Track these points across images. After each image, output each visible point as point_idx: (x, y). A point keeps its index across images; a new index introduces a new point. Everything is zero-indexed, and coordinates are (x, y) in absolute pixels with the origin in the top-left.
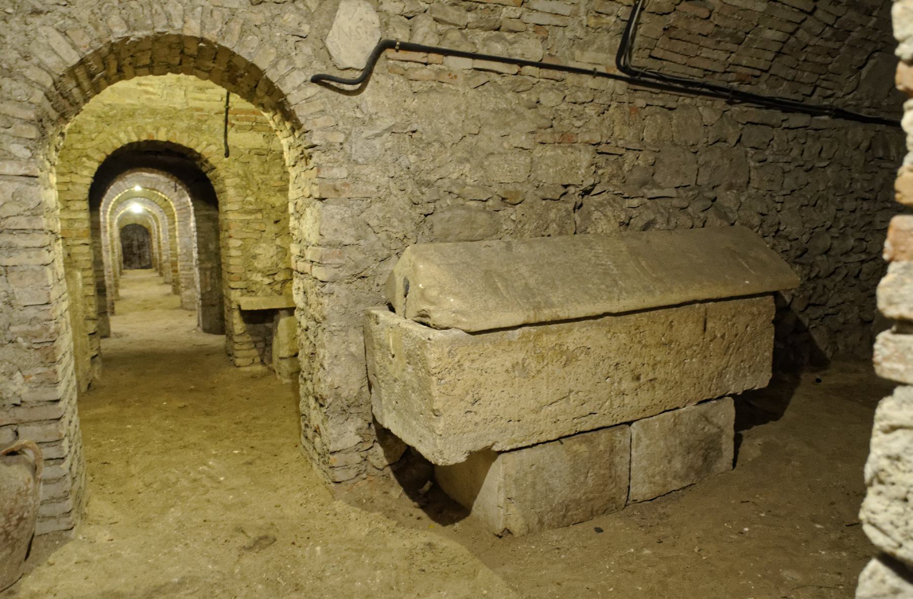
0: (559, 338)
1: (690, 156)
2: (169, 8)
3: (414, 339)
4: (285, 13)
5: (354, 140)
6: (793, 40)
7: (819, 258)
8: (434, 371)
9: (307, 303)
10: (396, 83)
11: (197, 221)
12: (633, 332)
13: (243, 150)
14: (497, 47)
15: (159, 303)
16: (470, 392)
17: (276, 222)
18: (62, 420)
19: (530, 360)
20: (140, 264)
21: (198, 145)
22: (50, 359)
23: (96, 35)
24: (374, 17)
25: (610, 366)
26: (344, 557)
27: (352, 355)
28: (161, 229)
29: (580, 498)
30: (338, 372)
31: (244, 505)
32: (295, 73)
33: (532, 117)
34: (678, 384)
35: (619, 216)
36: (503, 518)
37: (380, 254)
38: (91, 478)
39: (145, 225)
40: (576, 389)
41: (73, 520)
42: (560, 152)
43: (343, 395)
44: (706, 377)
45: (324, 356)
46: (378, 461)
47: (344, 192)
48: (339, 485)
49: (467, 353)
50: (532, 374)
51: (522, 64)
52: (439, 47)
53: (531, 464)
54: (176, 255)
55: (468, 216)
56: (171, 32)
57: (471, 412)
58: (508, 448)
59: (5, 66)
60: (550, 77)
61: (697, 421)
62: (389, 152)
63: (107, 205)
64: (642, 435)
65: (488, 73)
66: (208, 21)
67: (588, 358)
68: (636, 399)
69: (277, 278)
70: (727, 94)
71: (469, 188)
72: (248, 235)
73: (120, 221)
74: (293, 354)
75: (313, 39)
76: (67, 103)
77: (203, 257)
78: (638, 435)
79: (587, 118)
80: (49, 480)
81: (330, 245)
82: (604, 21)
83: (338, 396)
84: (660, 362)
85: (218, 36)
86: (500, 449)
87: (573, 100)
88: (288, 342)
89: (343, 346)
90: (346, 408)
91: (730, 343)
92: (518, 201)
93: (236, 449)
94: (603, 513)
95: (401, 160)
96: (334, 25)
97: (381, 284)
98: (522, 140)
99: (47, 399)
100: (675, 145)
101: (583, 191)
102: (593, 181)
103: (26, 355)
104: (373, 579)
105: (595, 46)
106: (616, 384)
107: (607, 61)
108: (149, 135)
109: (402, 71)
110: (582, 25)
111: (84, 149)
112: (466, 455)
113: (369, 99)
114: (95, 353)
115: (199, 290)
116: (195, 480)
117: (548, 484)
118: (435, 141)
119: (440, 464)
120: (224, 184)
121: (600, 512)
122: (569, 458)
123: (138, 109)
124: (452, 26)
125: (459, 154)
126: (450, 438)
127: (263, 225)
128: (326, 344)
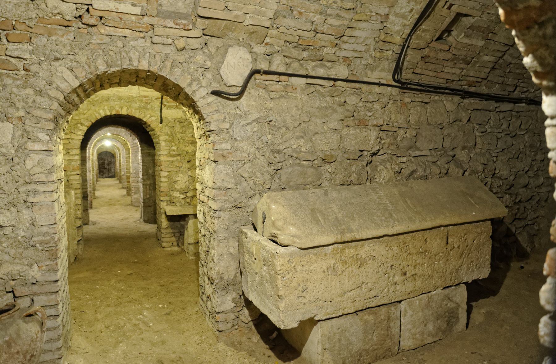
0: (356, 251)
1: (438, 131)
2: (131, 54)
3: (268, 251)
4: (197, 55)
5: (235, 127)
6: (501, 61)
7: (521, 190)
8: (279, 272)
9: (205, 220)
10: (261, 93)
11: (142, 156)
12: (402, 246)
14: (321, 71)
15: (119, 201)
16: (301, 285)
17: (189, 162)
19: (338, 264)
20: (109, 174)
21: (144, 117)
22: (54, 256)
23: (89, 70)
24: (248, 56)
27: (231, 254)
28: (121, 156)
29: (369, 348)
30: (222, 265)
31: (163, 343)
32: (201, 89)
33: (341, 111)
34: (431, 277)
37: (249, 194)
40: (367, 282)
41: (62, 353)
42: (358, 131)
43: (225, 278)
44: (448, 272)
45: (214, 255)
46: (245, 318)
48: (221, 333)
49: (300, 261)
50: (339, 273)
51: (335, 80)
53: (338, 327)
54: (129, 172)
56: (132, 67)
57: (301, 296)
58: (324, 318)
61: (443, 300)
62: (256, 134)
63: (91, 145)
64: (408, 309)
68: (404, 287)
69: (188, 194)
70: (461, 93)
71: (303, 154)
72: (172, 169)
73: (98, 150)
74: (196, 242)
75: (213, 69)
76: (71, 106)
77: (145, 177)
78: (405, 309)
79: (375, 111)
80: (50, 328)
81: (219, 188)
83: (222, 279)
84: (419, 264)
86: (319, 319)
89: (226, 249)
90: (227, 286)
91: (463, 251)
92: (332, 161)
94: (384, 358)
95: (262, 138)
96: (225, 63)
98: (335, 124)
99: (51, 280)
100: (429, 124)
101: (372, 153)
102: (378, 148)
103: (41, 254)
105: (380, 69)
106: (391, 278)
107: (387, 77)
108: (117, 111)
109: (264, 86)
110: (372, 57)
111: (79, 119)
112: (298, 322)
115: (142, 197)
116: (135, 325)
117: (348, 340)
118: (283, 126)
119: (282, 328)
120: (159, 139)
121: (381, 357)
122: (362, 323)
123: (111, 97)
124: (294, 60)
125: (297, 134)
126: (289, 313)
128: (216, 247)
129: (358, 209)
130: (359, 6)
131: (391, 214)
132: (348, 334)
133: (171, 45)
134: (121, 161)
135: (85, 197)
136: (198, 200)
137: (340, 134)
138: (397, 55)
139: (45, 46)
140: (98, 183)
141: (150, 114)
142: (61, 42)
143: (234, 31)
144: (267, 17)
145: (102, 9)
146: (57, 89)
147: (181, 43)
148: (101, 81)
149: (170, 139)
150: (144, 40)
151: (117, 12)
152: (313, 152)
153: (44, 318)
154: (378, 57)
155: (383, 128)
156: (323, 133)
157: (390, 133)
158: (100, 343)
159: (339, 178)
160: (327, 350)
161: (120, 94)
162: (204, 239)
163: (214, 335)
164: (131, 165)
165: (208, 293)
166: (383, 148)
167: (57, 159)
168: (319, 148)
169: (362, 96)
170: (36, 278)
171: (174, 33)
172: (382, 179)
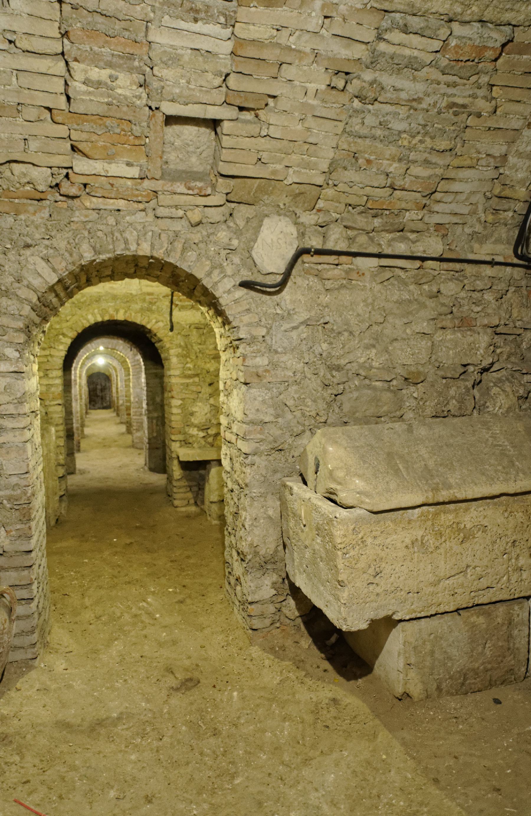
0: (456, 517)
2: (127, 235)
3: (323, 515)
4: (219, 231)
5: (274, 333)
8: (340, 546)
9: (232, 468)
11: (147, 379)
13: (185, 326)
14: (401, 247)
15: (115, 441)
16: (372, 566)
17: (210, 385)
18: (34, 566)
20: (102, 404)
21: (148, 323)
23: (70, 260)
24: (292, 230)
25: (507, 543)
26: (258, 705)
27: (270, 518)
28: (119, 378)
31: (174, 642)
32: (226, 280)
33: (433, 305)
35: (518, 391)
36: (402, 682)
37: (295, 430)
38: (54, 608)
39: (107, 373)
40: (473, 565)
42: (459, 335)
43: (260, 553)
45: (246, 518)
46: (290, 613)
47: (265, 377)
48: (255, 632)
50: (430, 550)
51: (423, 259)
52: (349, 250)
53: (429, 633)
54: (129, 401)
55: (374, 395)
56: (128, 253)
57: (373, 583)
58: (407, 618)
59: (3, 288)
60: (450, 269)
62: (304, 342)
63: (77, 364)
65: (392, 269)
66: (157, 243)
67: (485, 536)
69: (210, 432)
71: (375, 370)
72: (187, 396)
73: (87, 371)
76: (47, 310)
79: (485, 304)
80: (22, 617)
81: (252, 423)
82: (501, 217)
83: (256, 553)
85: (164, 254)
86: (400, 618)
87: (472, 289)
88: (217, 489)
89: (262, 510)
90: (263, 564)
92: (419, 381)
93: (170, 588)
94: (502, 684)
95: (314, 348)
96: (259, 240)
97: (295, 455)
98: (424, 326)
101: (482, 369)
102: (491, 360)
103: (8, 514)
104: (282, 731)
106: (513, 561)
108: (111, 316)
109: (316, 272)
110: (480, 222)
112: (368, 622)
113: (288, 297)
114: (63, 493)
115: (147, 435)
116: (136, 616)
117: (445, 652)
118: (345, 330)
119: (344, 630)
120: (168, 354)
122: (467, 628)
125: (366, 341)
126: (354, 607)
127: (199, 387)
128: (248, 508)
129: (460, 452)
130: (459, 145)
131: (512, 462)
132: (445, 645)
133: (181, 218)
134: (119, 386)
135: (70, 435)
136: (223, 440)
137: (431, 340)
138: (521, 216)
139: (11, 229)
140: (87, 416)
141: (156, 318)
142: (33, 222)
143: (271, 193)
144: (318, 170)
145: (87, 173)
146: (28, 287)
147: (195, 216)
148: (87, 274)
149: (185, 352)
150: (144, 213)
151: (106, 177)
152: (389, 368)
153: (13, 601)
154: (491, 221)
155: (499, 330)
156: (405, 339)
157: (511, 338)
158: (87, 639)
159: (430, 406)
160: (412, 667)
161: (115, 292)
162: (231, 495)
163: (245, 636)
164: (131, 390)
165: (237, 574)
166: (498, 361)
167: (30, 383)
168: (399, 361)
169: (466, 281)
170: (3, 547)
171: (185, 202)
172: (497, 409)
